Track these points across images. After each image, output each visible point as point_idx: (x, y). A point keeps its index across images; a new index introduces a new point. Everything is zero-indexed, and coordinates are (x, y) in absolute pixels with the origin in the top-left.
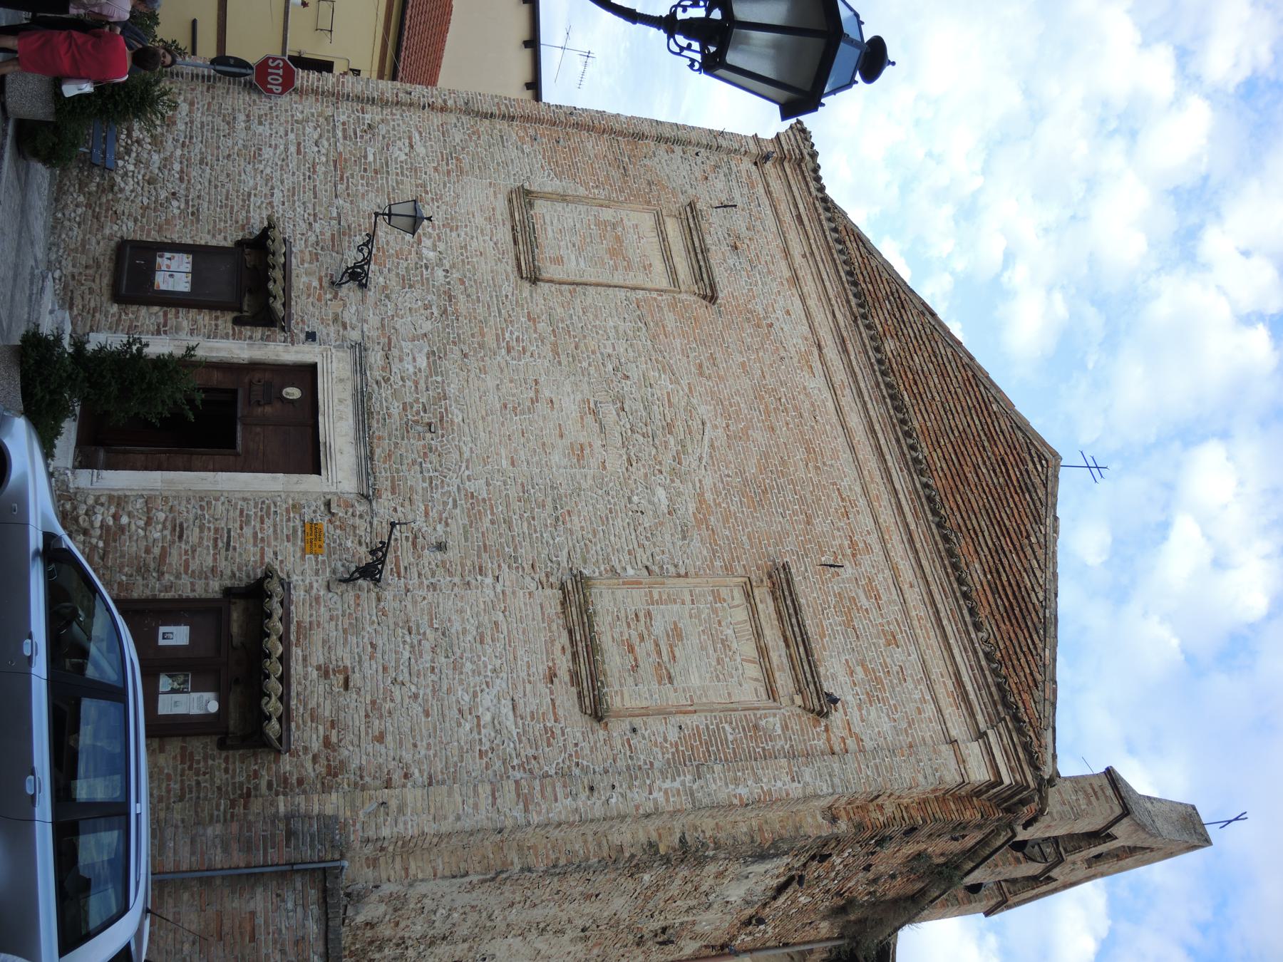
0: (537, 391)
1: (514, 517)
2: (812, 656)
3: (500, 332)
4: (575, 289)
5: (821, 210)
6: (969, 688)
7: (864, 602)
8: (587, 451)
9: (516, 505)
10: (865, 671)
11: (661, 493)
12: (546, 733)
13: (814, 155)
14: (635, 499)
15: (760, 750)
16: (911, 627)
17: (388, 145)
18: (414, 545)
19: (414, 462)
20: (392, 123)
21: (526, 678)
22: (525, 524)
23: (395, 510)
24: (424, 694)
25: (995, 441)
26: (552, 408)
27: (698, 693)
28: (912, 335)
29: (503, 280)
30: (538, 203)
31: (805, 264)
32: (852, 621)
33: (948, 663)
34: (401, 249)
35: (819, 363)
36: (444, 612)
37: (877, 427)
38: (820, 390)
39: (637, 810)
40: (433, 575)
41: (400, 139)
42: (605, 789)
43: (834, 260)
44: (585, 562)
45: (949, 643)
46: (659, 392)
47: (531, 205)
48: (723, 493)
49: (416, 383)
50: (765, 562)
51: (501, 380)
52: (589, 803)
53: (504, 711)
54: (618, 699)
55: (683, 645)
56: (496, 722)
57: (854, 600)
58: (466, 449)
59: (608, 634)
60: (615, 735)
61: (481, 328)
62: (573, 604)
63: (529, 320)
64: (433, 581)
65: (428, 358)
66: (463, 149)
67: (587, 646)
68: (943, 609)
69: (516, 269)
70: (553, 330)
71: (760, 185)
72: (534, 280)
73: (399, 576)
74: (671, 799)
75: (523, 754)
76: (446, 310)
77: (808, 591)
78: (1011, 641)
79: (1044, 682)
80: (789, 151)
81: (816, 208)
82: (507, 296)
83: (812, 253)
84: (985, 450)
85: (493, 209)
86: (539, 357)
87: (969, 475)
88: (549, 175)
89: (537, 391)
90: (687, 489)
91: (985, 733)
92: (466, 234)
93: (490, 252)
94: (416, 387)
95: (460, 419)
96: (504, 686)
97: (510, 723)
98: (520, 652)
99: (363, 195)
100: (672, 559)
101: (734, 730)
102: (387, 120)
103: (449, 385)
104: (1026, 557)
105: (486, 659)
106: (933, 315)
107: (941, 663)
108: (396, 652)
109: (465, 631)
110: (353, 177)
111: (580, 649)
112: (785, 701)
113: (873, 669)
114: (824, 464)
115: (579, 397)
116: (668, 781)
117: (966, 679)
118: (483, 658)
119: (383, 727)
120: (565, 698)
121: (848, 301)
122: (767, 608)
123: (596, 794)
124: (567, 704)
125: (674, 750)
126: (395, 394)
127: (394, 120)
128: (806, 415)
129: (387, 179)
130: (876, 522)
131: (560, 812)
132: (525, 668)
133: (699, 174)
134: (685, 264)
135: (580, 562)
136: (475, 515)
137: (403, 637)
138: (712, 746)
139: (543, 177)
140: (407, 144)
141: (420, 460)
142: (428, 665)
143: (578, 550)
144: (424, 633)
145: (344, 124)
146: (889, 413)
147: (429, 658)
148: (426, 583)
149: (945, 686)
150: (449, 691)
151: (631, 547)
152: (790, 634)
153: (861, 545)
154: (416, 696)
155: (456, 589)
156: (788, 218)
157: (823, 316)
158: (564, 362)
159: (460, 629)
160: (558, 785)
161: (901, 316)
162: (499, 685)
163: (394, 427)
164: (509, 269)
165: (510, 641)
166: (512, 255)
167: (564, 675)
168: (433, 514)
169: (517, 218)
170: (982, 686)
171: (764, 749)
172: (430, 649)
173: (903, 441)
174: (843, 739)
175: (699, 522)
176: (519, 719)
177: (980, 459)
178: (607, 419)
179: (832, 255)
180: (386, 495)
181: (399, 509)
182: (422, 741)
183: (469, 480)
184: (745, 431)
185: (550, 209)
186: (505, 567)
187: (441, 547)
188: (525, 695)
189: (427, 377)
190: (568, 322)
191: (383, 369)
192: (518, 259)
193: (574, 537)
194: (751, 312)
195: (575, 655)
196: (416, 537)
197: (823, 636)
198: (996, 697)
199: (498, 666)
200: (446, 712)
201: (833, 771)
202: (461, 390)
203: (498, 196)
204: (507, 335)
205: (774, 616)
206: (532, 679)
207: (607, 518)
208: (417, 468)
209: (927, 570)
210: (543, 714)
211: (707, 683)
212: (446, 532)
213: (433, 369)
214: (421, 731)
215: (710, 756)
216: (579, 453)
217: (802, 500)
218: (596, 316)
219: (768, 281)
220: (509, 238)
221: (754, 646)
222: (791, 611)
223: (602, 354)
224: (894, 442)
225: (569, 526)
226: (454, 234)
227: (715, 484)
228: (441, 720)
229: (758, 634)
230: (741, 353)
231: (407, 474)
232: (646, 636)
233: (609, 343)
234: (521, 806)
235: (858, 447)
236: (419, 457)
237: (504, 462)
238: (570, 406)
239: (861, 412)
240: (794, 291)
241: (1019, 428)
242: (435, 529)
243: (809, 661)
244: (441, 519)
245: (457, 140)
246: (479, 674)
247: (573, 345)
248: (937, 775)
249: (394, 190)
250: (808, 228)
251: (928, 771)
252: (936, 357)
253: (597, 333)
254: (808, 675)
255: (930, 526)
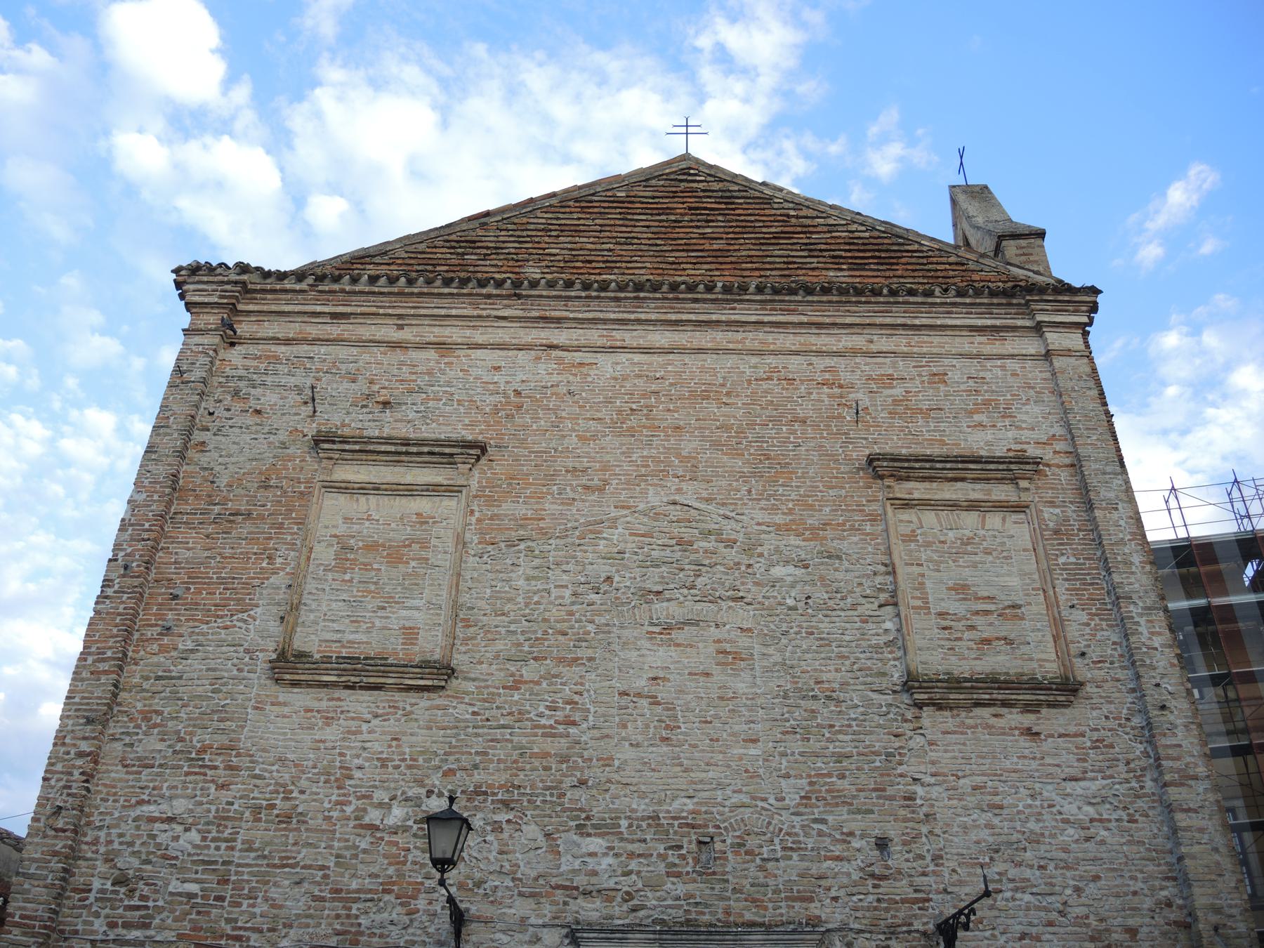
0: (639, 695)
1: (831, 749)
2: (982, 457)
3: (540, 731)
4: (462, 620)
5: (336, 287)
6: (989, 322)
7: (898, 391)
8: (728, 647)
9: (814, 745)
10: (978, 413)
11: (778, 571)
12: (1099, 748)
13: (243, 268)
14: (790, 602)
15: (1081, 533)
16: (923, 355)
17: (165, 857)
18: (884, 878)
19: (761, 868)
20: (116, 846)
21: (1038, 762)
22: (841, 737)
23: (835, 899)
24: (1073, 879)
25: (667, 208)
26: (664, 679)
27: (1028, 581)
28: (516, 245)
29: (445, 715)
30: (298, 644)
31: (415, 329)
32: (921, 409)
33: (958, 333)
34: (385, 856)
35: (575, 354)
36: (969, 848)
37: (673, 317)
38: (617, 364)
39: (1175, 665)
40: (922, 857)
41: (153, 837)
42: (1160, 694)
43: (421, 294)
44: (884, 674)
45: (940, 326)
46: (629, 545)
47: (301, 655)
48: (773, 502)
49: (631, 855)
50: (861, 478)
51: (624, 739)
52: (1176, 713)
53: (1080, 791)
54: (1047, 665)
55: (974, 585)
56: (1094, 801)
57: (895, 401)
58: (736, 799)
59: (968, 664)
60: (1089, 676)
61: (533, 755)
62: (946, 696)
63: (518, 689)
64: (929, 858)
65: (589, 835)
66: (181, 740)
67: (999, 688)
68: (903, 320)
69: (426, 694)
70: (535, 659)
71: (273, 348)
72: (448, 671)
73: (929, 900)
74: (1158, 630)
75: (1124, 776)
76: (503, 802)
77: (895, 444)
78: (916, 270)
79: (958, 256)
80: (221, 297)
81: (330, 292)
82: (474, 713)
83: (400, 316)
84: (680, 222)
85: (308, 710)
86: (582, 684)
87: (715, 247)
88: (245, 621)
89: (639, 695)
90: (770, 542)
91: (1039, 323)
92: (358, 756)
93: (392, 725)
94: (640, 856)
95: (688, 801)
96: (1050, 787)
97: (1093, 786)
98: (1008, 764)
99: (272, 906)
100: (868, 576)
101: (1063, 554)
102: (107, 853)
103: (633, 811)
104: (814, 226)
105: (1021, 805)
106: (487, 214)
107: (958, 340)
108: (1028, 909)
109: (989, 826)
110: (236, 920)
111: (1000, 697)
112: (1025, 497)
113: (974, 404)
114: (723, 385)
115: (644, 643)
116: (1140, 629)
117: (979, 322)
118: (1021, 808)
119: (1119, 929)
120: (1054, 721)
121: (489, 296)
122: (918, 490)
123: (1168, 704)
124: (1062, 721)
125: (1096, 618)
126: (654, 888)
127: (110, 842)
128: (654, 387)
129: (239, 865)
130: (797, 353)
131: (1191, 743)
132: (1026, 762)
133: (250, 420)
134: (417, 471)
135: (885, 680)
136: (833, 797)
137: (1007, 900)
138: (1086, 579)
139: (247, 630)
140: (165, 826)
141: (758, 861)
142: (1038, 873)
143: (869, 679)
144: (999, 874)
145: (112, 925)
146: (659, 299)
147: (1028, 871)
148: (932, 868)
149: (980, 343)
150: (1066, 851)
151: (857, 619)
152: (950, 474)
153: (827, 376)
154: (1078, 890)
155: (937, 831)
156: (334, 330)
157: (500, 331)
158: (590, 653)
159: (987, 831)
160: (1164, 741)
161: (488, 248)
162: (1049, 792)
163: (708, 892)
164: (424, 703)
165: (995, 775)
166: (398, 696)
167: (1028, 720)
168: (837, 850)
169: (334, 679)
170: (989, 309)
171: (1079, 530)
172: (1017, 870)
173: (699, 296)
174: (1055, 452)
175: (815, 537)
176: (1087, 775)
177: (695, 230)
178: (676, 614)
179: (412, 294)
180: (814, 909)
181: (833, 893)
182: (1129, 885)
183: (783, 799)
184: (683, 459)
185: (311, 630)
186: (900, 770)
187: (882, 844)
188: (1058, 766)
189: (622, 840)
190: (522, 638)
191: (610, 900)
192: (410, 688)
193: (852, 681)
194: (496, 411)
195: (1006, 704)
196: (873, 876)
197: (943, 443)
198: (1004, 301)
199: (1028, 792)
200: (1091, 855)
201: (1098, 469)
202: (643, 795)
203: (281, 699)
204: (543, 721)
205: (927, 485)
206: (1038, 756)
207: (821, 639)
208: (770, 865)
209: (858, 320)
210: (1077, 748)
211: (1014, 570)
212: (862, 837)
213: (606, 828)
214: (1117, 886)
215: (1097, 584)
216: (730, 657)
217: (776, 421)
218: (510, 600)
219: (443, 379)
220: (366, 696)
221: (965, 513)
222: (927, 465)
223: (573, 603)
224: (697, 306)
225: (836, 686)
226: (358, 774)
227: (762, 509)
228: (1100, 862)
229: (954, 505)
230: (564, 437)
231: (780, 880)
232: (969, 623)
233: (555, 593)
234: (1192, 783)
235: (704, 344)
236: (753, 861)
237: (752, 752)
238: (659, 657)
239: (646, 327)
240: (458, 352)
241: (647, 180)
242: (858, 850)
243: (986, 462)
244: (844, 841)
245: (160, 746)
246: (1040, 814)
247: (560, 637)
248: (1085, 377)
249: (265, 857)
250: (359, 310)
251: (1082, 384)
252: (551, 230)
253: (537, 603)
254: (1001, 467)
255: (808, 302)
